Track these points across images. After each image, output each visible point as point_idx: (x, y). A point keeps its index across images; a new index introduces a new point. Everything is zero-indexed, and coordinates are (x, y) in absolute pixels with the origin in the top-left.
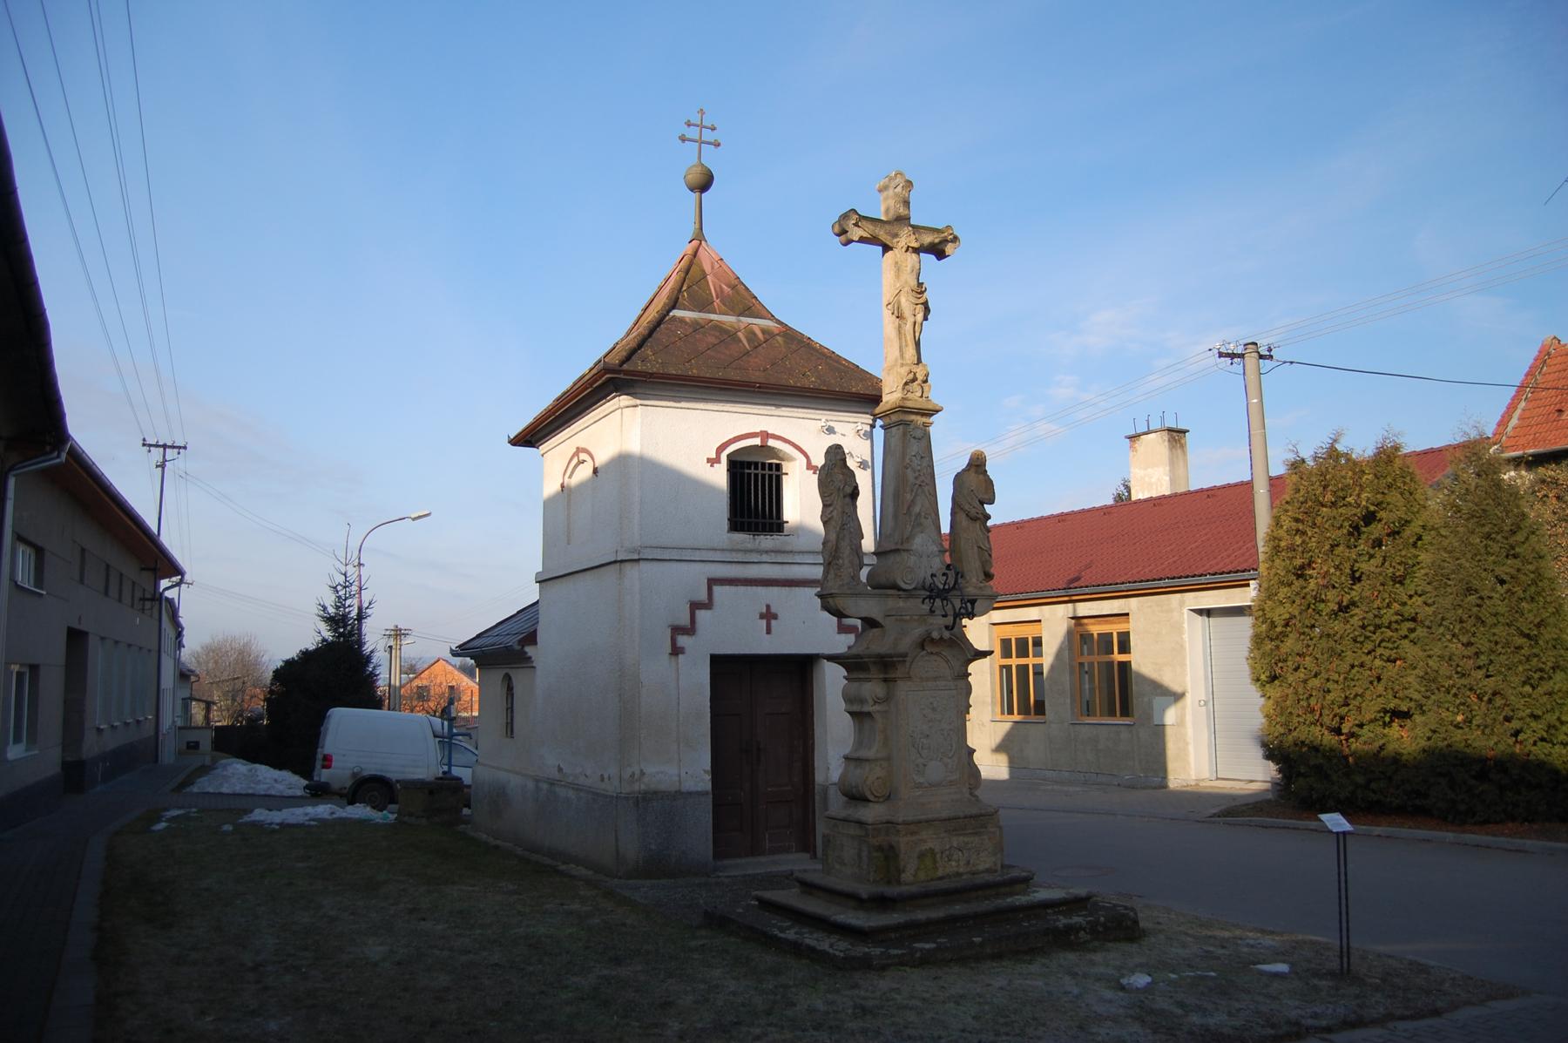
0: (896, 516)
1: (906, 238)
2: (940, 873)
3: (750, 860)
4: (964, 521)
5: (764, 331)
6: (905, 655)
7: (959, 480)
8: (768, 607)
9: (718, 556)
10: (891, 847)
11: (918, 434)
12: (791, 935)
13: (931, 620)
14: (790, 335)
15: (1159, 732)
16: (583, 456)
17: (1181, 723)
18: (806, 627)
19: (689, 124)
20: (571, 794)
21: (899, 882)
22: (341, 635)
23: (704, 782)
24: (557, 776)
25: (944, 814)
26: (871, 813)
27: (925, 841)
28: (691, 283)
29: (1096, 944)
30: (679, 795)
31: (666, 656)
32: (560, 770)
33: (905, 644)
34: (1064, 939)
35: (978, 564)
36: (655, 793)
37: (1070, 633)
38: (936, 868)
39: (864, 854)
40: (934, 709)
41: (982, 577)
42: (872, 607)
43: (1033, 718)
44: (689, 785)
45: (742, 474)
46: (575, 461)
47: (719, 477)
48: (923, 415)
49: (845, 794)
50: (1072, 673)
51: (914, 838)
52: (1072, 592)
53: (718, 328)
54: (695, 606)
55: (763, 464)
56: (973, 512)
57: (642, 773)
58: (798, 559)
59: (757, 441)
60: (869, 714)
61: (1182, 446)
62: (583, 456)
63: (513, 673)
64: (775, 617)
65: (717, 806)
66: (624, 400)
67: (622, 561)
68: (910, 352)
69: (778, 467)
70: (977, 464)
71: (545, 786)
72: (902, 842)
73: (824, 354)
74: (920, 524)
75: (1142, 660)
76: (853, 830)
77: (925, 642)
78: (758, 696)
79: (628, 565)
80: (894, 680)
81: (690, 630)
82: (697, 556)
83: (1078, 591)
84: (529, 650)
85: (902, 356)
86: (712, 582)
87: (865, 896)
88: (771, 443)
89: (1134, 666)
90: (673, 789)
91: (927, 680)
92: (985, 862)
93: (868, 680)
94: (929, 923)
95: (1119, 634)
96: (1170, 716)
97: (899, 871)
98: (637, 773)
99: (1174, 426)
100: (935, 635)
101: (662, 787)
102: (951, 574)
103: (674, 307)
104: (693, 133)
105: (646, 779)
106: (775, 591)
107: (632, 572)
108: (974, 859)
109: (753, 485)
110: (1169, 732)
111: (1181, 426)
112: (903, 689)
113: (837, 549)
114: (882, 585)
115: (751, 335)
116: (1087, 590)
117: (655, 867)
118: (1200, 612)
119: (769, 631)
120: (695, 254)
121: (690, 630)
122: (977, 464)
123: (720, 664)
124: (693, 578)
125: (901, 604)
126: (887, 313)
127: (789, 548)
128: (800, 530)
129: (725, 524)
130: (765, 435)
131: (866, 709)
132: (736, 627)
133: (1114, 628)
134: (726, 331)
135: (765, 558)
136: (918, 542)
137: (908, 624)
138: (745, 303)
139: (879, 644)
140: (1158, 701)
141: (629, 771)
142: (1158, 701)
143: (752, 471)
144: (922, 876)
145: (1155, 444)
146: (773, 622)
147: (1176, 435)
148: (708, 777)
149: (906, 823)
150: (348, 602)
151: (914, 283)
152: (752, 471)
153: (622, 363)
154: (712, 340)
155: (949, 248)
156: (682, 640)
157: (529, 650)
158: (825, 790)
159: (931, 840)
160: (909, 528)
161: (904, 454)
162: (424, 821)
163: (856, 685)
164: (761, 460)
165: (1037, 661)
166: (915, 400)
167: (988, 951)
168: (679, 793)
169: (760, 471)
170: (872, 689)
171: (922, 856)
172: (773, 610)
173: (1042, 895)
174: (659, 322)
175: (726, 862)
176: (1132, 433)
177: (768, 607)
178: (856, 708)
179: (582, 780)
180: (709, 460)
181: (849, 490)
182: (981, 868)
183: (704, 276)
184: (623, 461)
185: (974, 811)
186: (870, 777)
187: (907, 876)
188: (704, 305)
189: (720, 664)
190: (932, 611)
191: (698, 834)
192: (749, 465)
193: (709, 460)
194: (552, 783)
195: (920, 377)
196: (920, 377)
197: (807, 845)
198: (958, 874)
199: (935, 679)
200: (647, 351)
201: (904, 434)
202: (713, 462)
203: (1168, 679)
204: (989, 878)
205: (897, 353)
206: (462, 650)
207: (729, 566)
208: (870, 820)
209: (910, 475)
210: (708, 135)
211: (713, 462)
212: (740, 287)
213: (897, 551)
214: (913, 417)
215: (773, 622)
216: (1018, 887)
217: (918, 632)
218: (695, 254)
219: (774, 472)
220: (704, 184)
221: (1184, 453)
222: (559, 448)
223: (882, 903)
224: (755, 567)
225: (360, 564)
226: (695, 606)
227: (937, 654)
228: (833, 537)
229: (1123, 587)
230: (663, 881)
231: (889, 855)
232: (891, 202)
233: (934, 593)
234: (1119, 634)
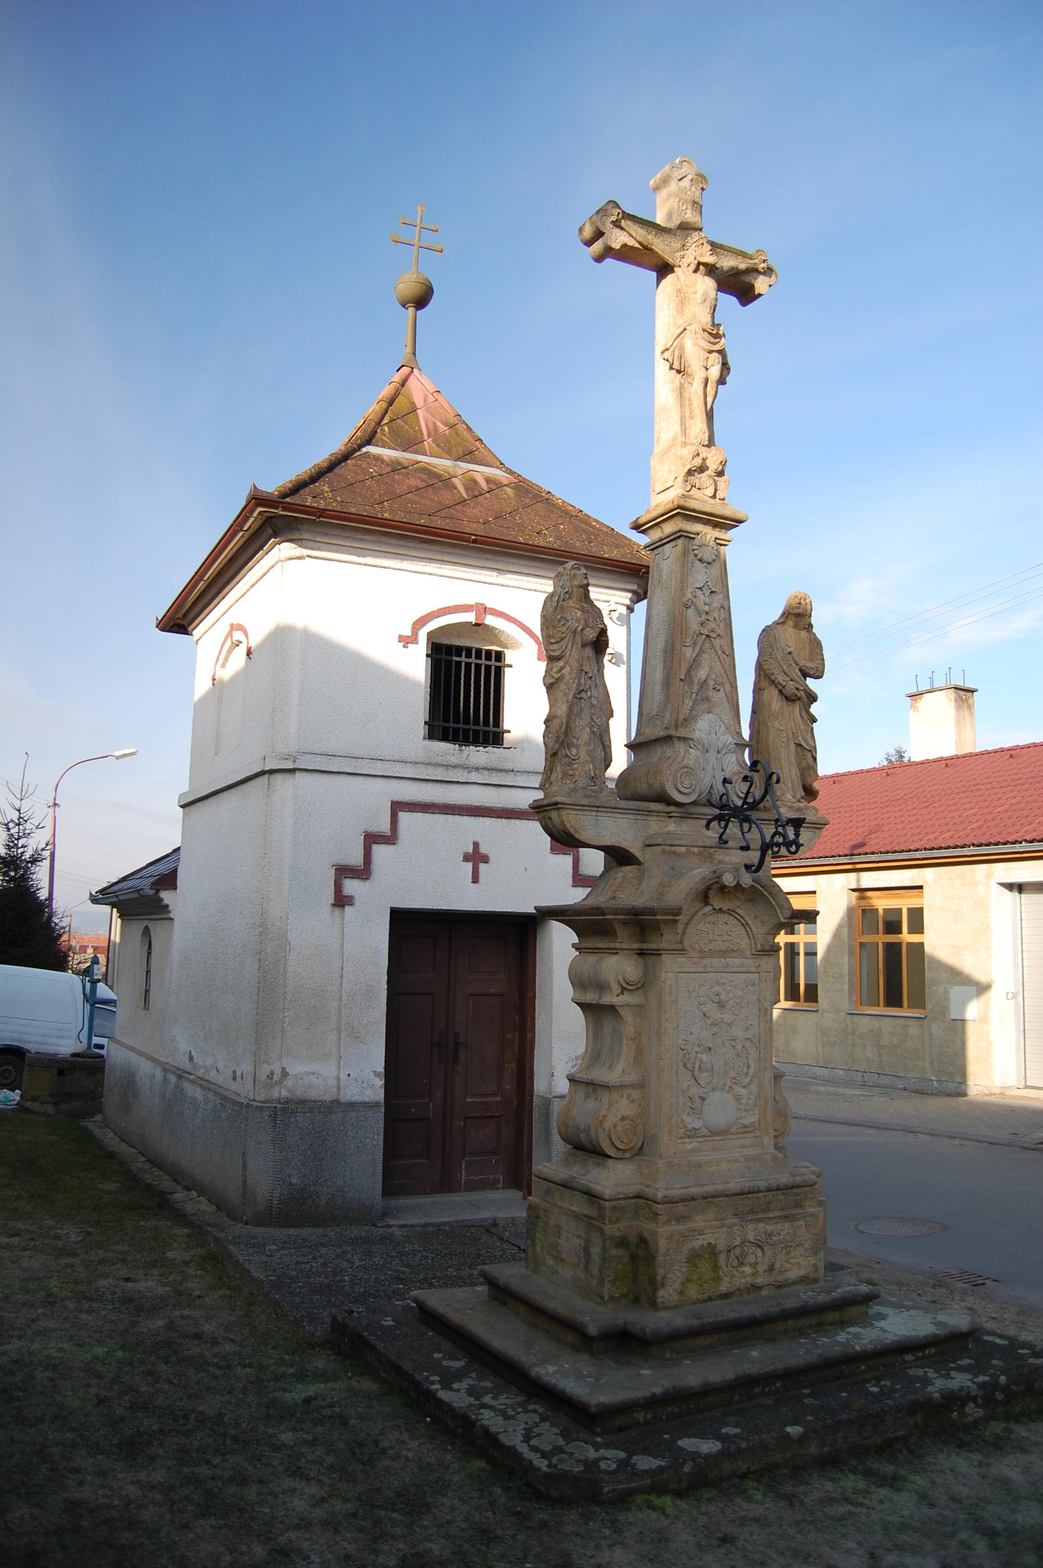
0: (667, 685)
1: (697, 251)
2: (724, 1287)
3: (439, 1198)
4: (774, 700)
5: (488, 481)
6: (677, 912)
7: (767, 638)
8: (476, 845)
9: (409, 771)
10: (642, 1241)
11: (708, 556)
12: (457, 1397)
13: (720, 855)
14: (523, 488)
15: (959, 1026)
16: (238, 635)
17: (984, 1019)
18: (528, 875)
20: (198, 1094)
21: (654, 1305)
22: (12, 879)
23: (375, 1090)
24: (188, 1067)
25: (734, 1185)
26: (611, 1179)
27: (701, 1233)
28: (393, 420)
29: (997, 1427)
30: (336, 1106)
31: (328, 908)
32: (191, 1058)
33: (679, 893)
34: (941, 1422)
35: (795, 772)
36: (302, 1102)
37: (850, 911)
38: (718, 1279)
39: (595, 1250)
40: (721, 1005)
41: (801, 793)
42: (622, 830)
43: (802, 1005)
44: (351, 1093)
45: (449, 663)
46: (229, 643)
47: (415, 664)
48: (716, 525)
49: (567, 1140)
50: (851, 953)
51: (681, 1227)
52: (856, 859)
53: (428, 471)
54: (371, 839)
55: (479, 652)
56: (790, 687)
57: (285, 1074)
59: (470, 617)
60: (612, 1009)
61: (970, 707)
62: (238, 635)
63: (152, 925)
64: (485, 859)
65: (390, 1119)
66: (285, 549)
67: (271, 772)
68: (698, 427)
69: (499, 656)
70: (797, 616)
71: (173, 1079)
72: (664, 1234)
73: (567, 513)
74: (707, 699)
75: (938, 941)
76: (578, 1205)
77: (711, 891)
78: (455, 969)
79: (279, 778)
80: (657, 953)
81: (363, 872)
82: (379, 769)
83: (863, 858)
84: (166, 896)
85: (684, 432)
86: (397, 807)
87: (593, 1331)
88: (490, 620)
89: (928, 949)
90: (328, 1097)
91: (712, 954)
92: (799, 1265)
93: (614, 951)
94: (708, 1391)
95: (910, 910)
96: (972, 1011)
97: (654, 1285)
98: (278, 1072)
99: (960, 684)
100: (728, 879)
101: (313, 1095)
102: (758, 778)
103: (368, 442)
105: (289, 1083)
107: (283, 785)
108: (783, 1261)
109: (461, 687)
110: (971, 1030)
111: (969, 685)
112: (672, 970)
113: (568, 730)
114: (641, 793)
115: (471, 484)
116: (873, 858)
117: (296, 1210)
118: (1010, 887)
119: (475, 879)
120: (404, 383)
121: (363, 872)
122: (797, 616)
123: (406, 924)
124: (370, 801)
125: (672, 827)
126: (661, 368)
127: (508, 766)
128: (524, 743)
129: (421, 730)
130: (483, 610)
131: (607, 999)
132: (430, 873)
133: (904, 903)
134: (438, 476)
135: (474, 777)
136: (703, 727)
137: (682, 861)
138: (470, 450)
139: (631, 892)
140: (956, 992)
141: (266, 1069)
142: (956, 992)
143: (463, 659)
144: (693, 1292)
145: (943, 703)
146: (482, 867)
147: (964, 693)
148: (380, 1082)
149: (669, 1201)
150: (21, 842)
151: (706, 319)
152: (463, 659)
153: (285, 495)
154: (414, 482)
155: (761, 284)
156: (351, 886)
157: (166, 896)
158: (547, 1103)
159: (709, 1230)
160: (688, 703)
161: (683, 584)
162: (50, 1109)
163: (592, 959)
164: (475, 645)
165: (810, 939)
166: (702, 500)
167: (813, 1450)
168: (336, 1102)
169: (473, 660)
170: (618, 967)
171: (694, 1259)
172: (483, 850)
173: (897, 1324)
174: (344, 457)
175: (403, 1201)
176: (914, 691)
177: (476, 845)
178: (590, 997)
179: (212, 1076)
180: (401, 638)
181: (591, 634)
182: (793, 1274)
183: (414, 410)
184: (281, 636)
185: (784, 1179)
186: (613, 1115)
187: (667, 1294)
188: (411, 444)
189: (406, 924)
190: (723, 841)
191: (361, 1162)
192: (459, 650)
193: (401, 638)
194: (181, 1075)
195: (713, 465)
196: (713, 465)
197: (519, 1176)
198: (756, 1288)
199: (724, 954)
200: (323, 486)
201: (685, 554)
202: (407, 641)
203: (969, 965)
204: (807, 1296)
205: (677, 428)
206: (103, 896)
207: (430, 786)
208: (608, 1193)
209: (693, 619)
210: (428, 239)
211: (407, 641)
212: (461, 427)
213: (667, 739)
214: (698, 527)
215: (482, 867)
216: (855, 1311)
217: (698, 873)
218: (404, 383)
219: (493, 663)
220: (421, 300)
221: (972, 714)
222: (212, 628)
223: (624, 1343)
225: (55, 804)
226: (371, 839)
227: (729, 912)
228: (563, 709)
229: (917, 855)
230: (305, 1232)
231: (640, 1252)
232: (674, 202)
233: (726, 812)
234: (910, 910)
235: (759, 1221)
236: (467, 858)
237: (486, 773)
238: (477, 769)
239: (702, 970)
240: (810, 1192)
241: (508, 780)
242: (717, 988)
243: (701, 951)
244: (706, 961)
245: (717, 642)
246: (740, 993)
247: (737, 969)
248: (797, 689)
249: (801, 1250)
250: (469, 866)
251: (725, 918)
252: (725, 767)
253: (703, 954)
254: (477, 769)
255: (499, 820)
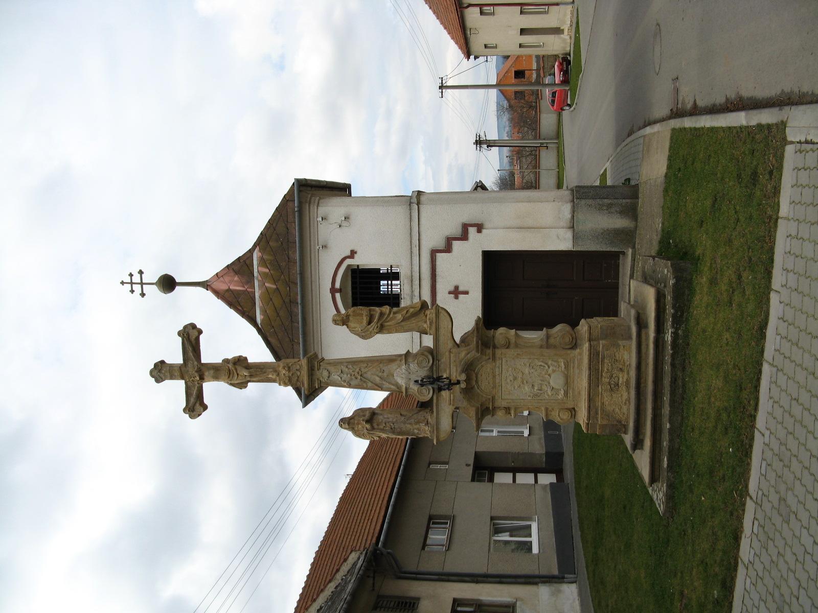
8: (450, 293)
19: (132, 291)
40: (515, 378)
58: (416, 268)
59: (338, 295)
64: (457, 288)
88: (338, 285)
91: (494, 382)
104: (137, 288)
106: (439, 286)
119: (466, 293)
130: (333, 291)
146: (461, 289)
172: (452, 289)
177: (450, 293)
215: (461, 289)
224: (423, 276)
235: (602, 375)
236: (457, 298)
237: (414, 287)
238: (412, 292)
239: (501, 387)
240: (594, 347)
241: (416, 275)
242: (508, 380)
243: (493, 388)
244: (497, 385)
245: (363, 370)
246: (510, 369)
247: (501, 370)
248: (377, 327)
249: (617, 354)
250: (461, 296)
251: (479, 376)
252: (416, 370)
253: (494, 387)
254: (412, 292)
255: (437, 280)
